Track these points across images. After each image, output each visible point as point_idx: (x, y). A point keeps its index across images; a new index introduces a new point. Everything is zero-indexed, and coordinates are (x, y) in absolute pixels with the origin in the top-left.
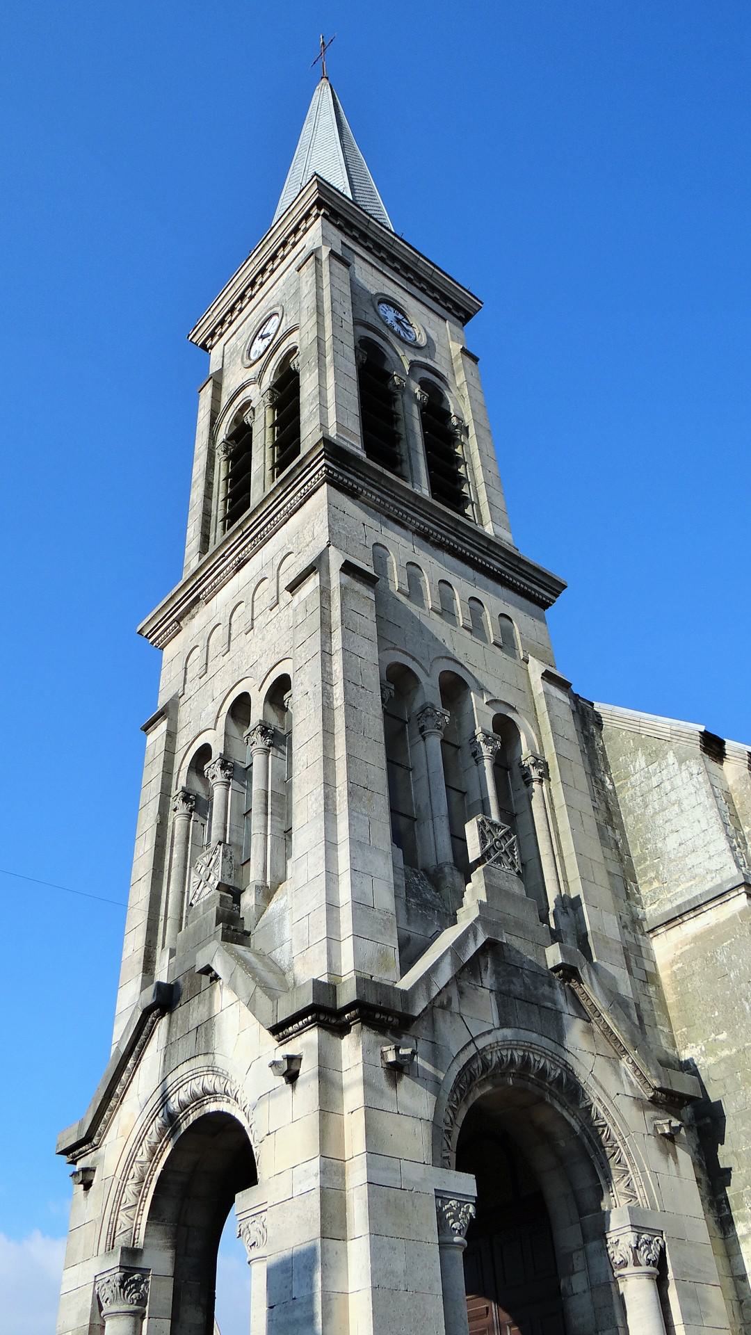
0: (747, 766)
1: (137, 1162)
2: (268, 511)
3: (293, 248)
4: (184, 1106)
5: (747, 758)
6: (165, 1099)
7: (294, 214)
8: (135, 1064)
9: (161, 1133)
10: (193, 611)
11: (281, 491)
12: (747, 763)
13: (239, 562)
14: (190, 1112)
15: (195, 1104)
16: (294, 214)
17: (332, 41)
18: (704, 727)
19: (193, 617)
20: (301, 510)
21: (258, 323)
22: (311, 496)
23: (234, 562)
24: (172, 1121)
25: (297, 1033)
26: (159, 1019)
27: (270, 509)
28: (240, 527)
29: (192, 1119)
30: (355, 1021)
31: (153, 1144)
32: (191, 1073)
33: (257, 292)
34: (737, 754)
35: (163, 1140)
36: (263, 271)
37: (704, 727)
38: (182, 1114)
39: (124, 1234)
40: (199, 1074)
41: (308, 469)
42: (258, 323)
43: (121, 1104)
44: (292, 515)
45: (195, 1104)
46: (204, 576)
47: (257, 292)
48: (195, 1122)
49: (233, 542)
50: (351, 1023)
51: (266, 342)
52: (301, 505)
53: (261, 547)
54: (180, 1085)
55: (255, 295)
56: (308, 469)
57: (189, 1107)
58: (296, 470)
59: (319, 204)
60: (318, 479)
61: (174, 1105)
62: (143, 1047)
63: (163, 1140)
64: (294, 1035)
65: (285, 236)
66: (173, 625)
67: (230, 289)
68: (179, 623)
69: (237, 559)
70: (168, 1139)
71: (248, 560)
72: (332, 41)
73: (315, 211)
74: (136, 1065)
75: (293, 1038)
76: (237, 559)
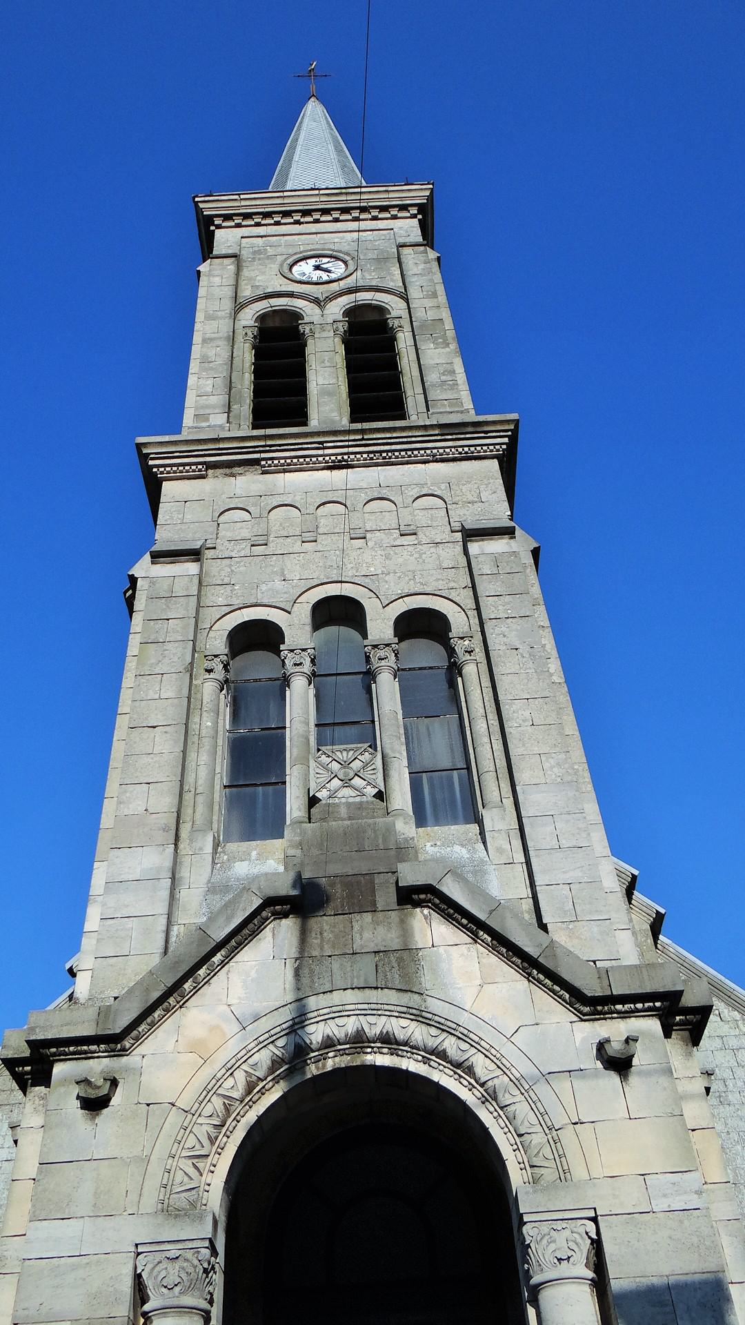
0: (650, 922)
1: (219, 1095)
2: (409, 439)
3: (371, 220)
4: (329, 1043)
5: (654, 916)
6: (298, 1023)
7: (391, 195)
8: (223, 961)
9: (275, 1063)
10: (236, 470)
11: (437, 432)
12: (652, 919)
13: (340, 461)
14: (331, 1055)
15: (348, 1046)
16: (391, 195)
17: (326, 76)
18: (638, 872)
19: (233, 475)
20: (451, 464)
21: (311, 250)
22: (471, 459)
23: (333, 458)
24: (299, 1054)
25: (622, 1015)
26: (274, 919)
27: (414, 439)
28: (363, 431)
29: (330, 1065)
30: (682, 1027)
31: (254, 1079)
32: (366, 1006)
33: (306, 223)
34: (644, 909)
35: (269, 1079)
36: (326, 212)
37: (638, 872)
38: (317, 1053)
39: (189, 1194)
40: (379, 1012)
41: (483, 435)
42: (311, 250)
43: (181, 1007)
44: (437, 461)
45: (348, 1046)
46: (280, 445)
47: (306, 223)
48: (336, 1071)
49: (343, 439)
50: (674, 1028)
51: (315, 276)
52: (454, 460)
53: (377, 465)
54: (333, 1015)
55: (303, 223)
56: (483, 435)
57: (333, 1049)
58: (467, 427)
59: (421, 208)
60: (491, 451)
61: (316, 1033)
62: (240, 946)
63: (269, 1079)
64: (615, 1015)
65: (370, 204)
66: (200, 467)
67: (278, 197)
68: (206, 470)
69: (339, 458)
70: (276, 1081)
71: (352, 467)
72: (326, 76)
73: (414, 211)
74: (223, 964)
75: (612, 1018)
76: (339, 458)
